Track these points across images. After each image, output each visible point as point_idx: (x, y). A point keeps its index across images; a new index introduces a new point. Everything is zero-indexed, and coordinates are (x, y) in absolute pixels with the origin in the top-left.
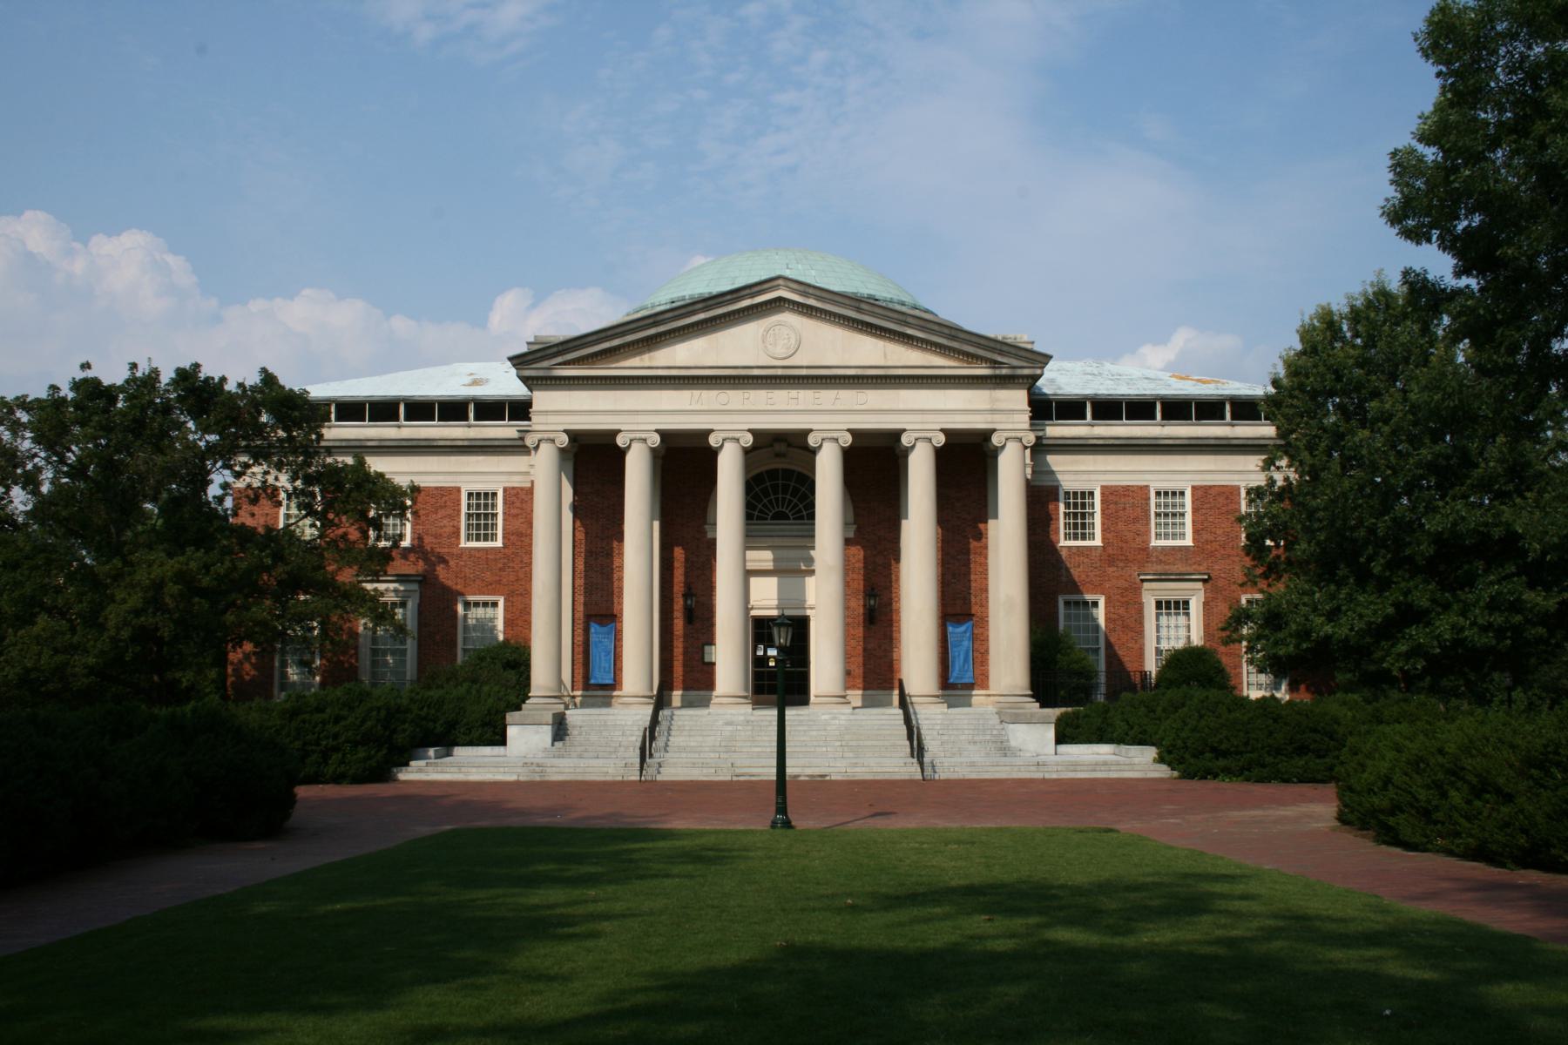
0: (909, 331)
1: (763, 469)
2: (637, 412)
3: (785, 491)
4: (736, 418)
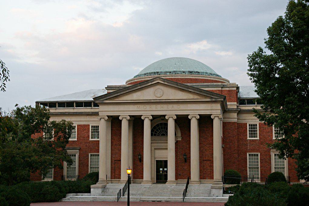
0: (190, 90)
1: (159, 123)
3: (162, 129)
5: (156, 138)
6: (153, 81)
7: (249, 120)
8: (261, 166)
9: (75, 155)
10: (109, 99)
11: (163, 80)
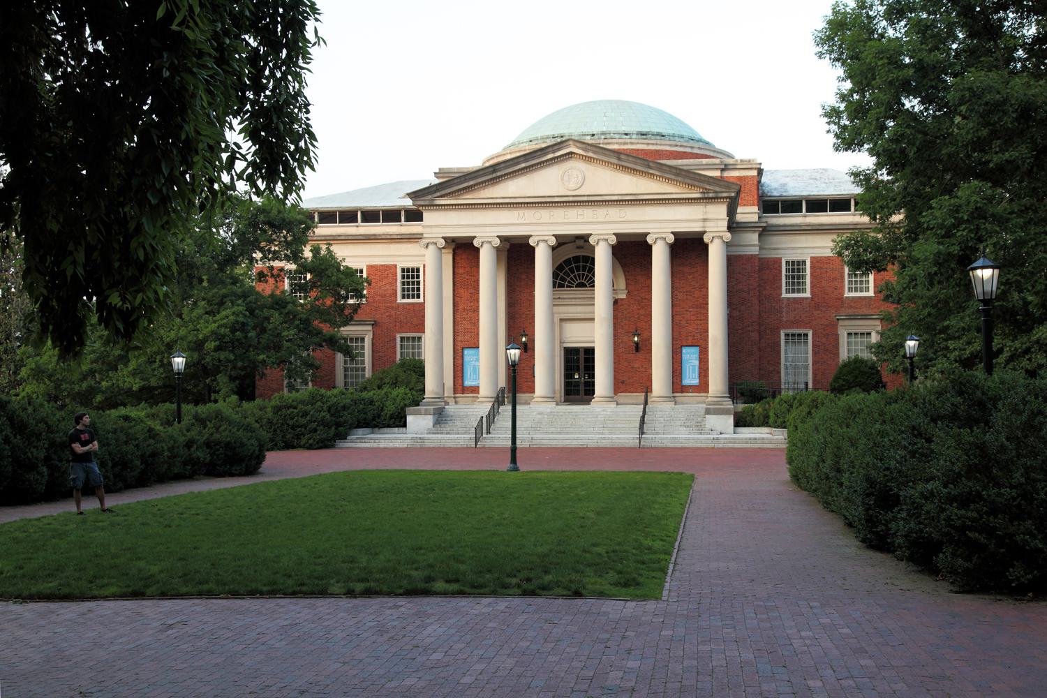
1: (561, 261)
2: (485, 225)
4: (545, 228)
5: (566, 293)
6: (559, 150)
7: (787, 252)
8: (814, 363)
9: (363, 340)
10: (449, 194)
11: (584, 146)
